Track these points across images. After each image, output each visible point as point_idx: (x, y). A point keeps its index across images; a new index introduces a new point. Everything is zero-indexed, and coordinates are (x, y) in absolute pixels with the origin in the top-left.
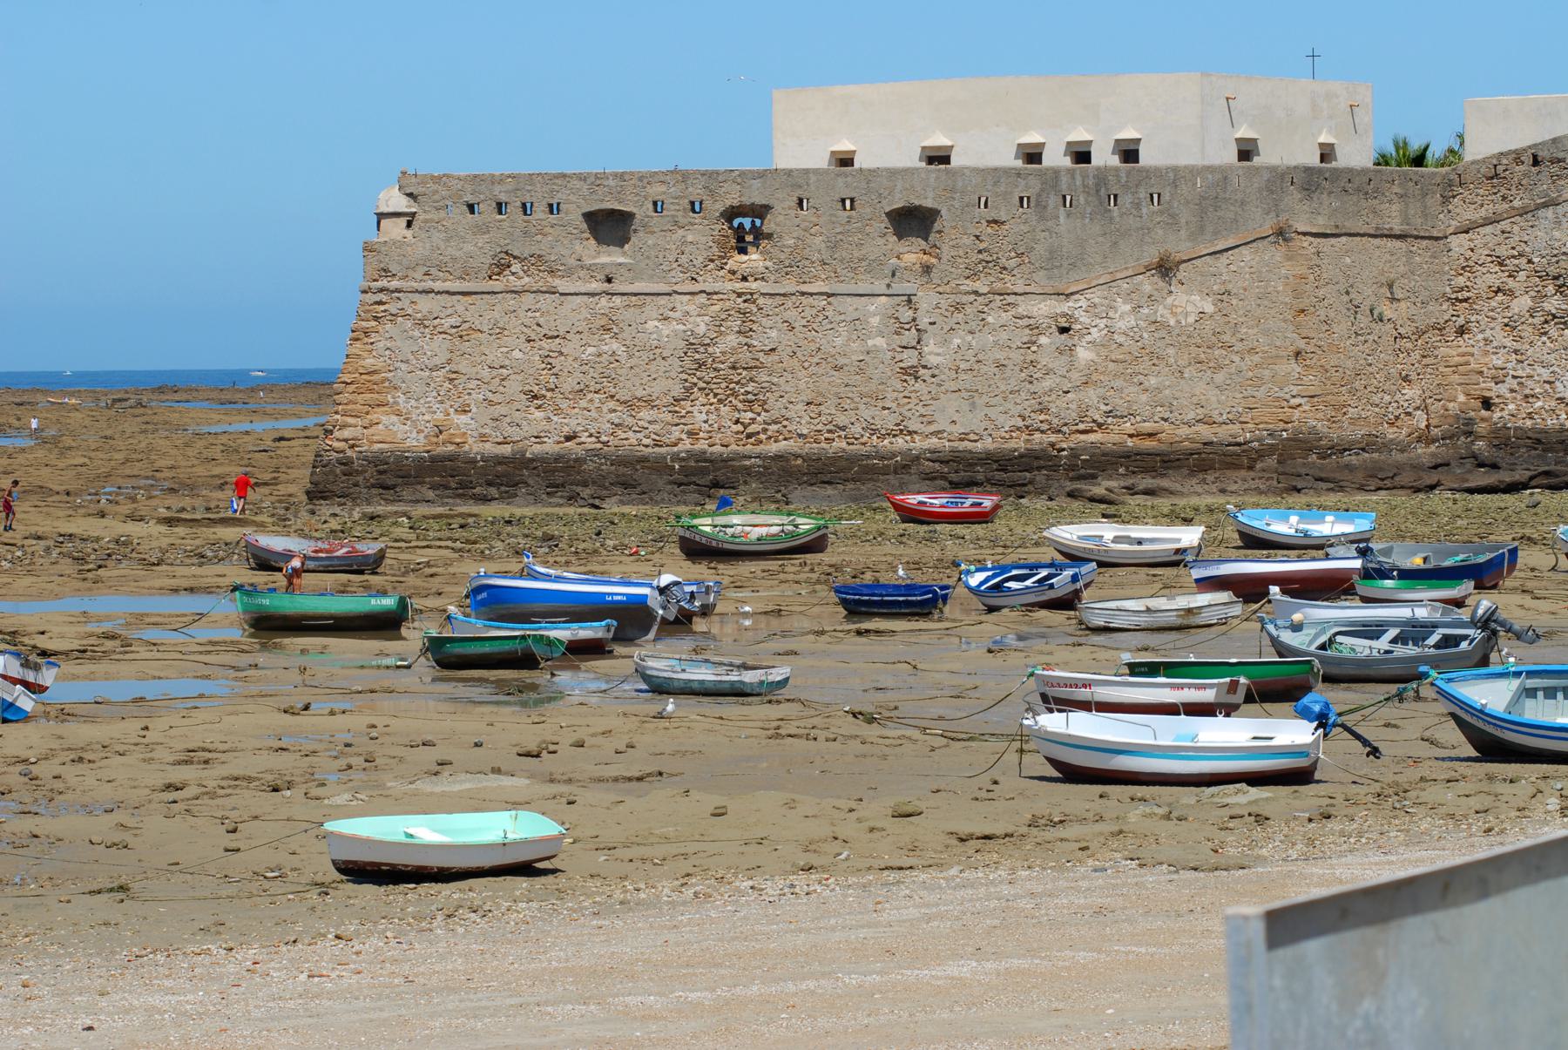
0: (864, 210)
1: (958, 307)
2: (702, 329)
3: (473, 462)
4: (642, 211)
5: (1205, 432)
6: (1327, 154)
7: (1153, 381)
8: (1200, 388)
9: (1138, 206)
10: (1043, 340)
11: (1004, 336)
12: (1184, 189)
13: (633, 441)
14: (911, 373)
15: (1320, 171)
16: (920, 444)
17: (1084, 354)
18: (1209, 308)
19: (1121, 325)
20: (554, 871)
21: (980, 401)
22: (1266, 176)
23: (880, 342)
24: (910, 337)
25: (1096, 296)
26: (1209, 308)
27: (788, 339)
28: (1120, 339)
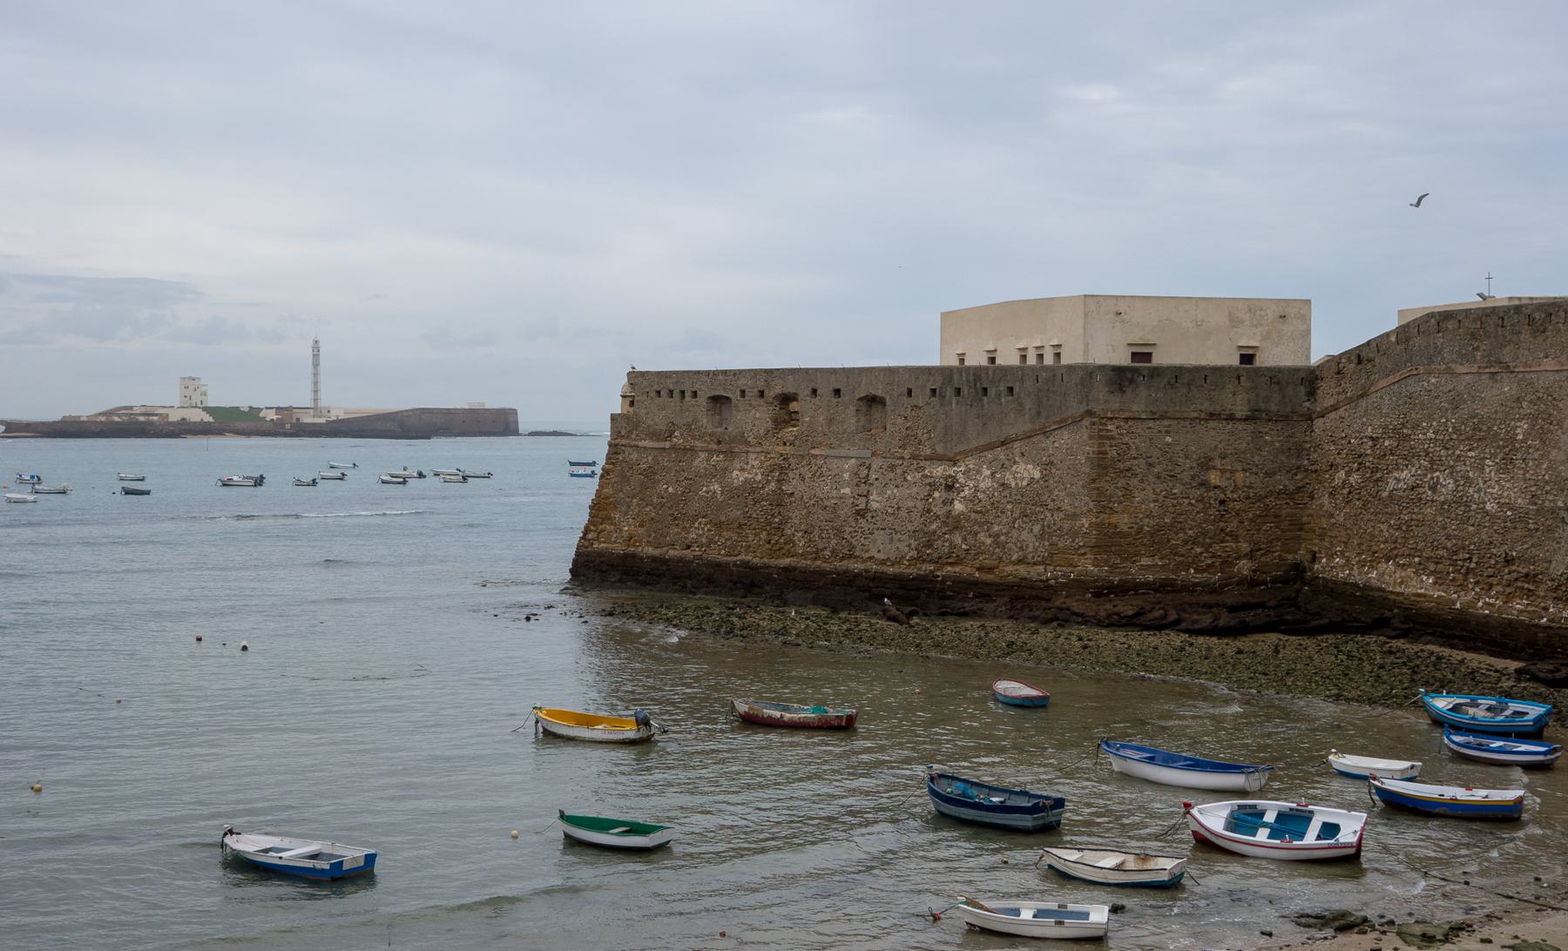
0: (845, 398)
1: (892, 467)
2: (759, 477)
3: (642, 559)
4: (735, 397)
5: (1022, 571)
6: (1247, 359)
7: (996, 528)
8: (1025, 535)
9: (999, 396)
10: (937, 494)
11: (915, 490)
12: (1029, 383)
13: (717, 554)
14: (861, 514)
15: (1133, 370)
16: (857, 566)
17: (959, 506)
18: (1037, 475)
19: (982, 485)
20: (148, 493)
21: (896, 537)
22: (1081, 373)
23: (847, 491)
24: (863, 489)
25: (971, 463)
26: (1037, 475)
27: (801, 487)
28: (981, 496)
